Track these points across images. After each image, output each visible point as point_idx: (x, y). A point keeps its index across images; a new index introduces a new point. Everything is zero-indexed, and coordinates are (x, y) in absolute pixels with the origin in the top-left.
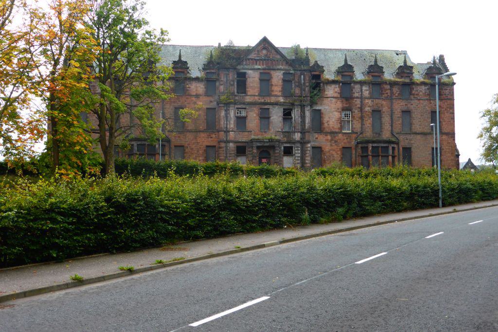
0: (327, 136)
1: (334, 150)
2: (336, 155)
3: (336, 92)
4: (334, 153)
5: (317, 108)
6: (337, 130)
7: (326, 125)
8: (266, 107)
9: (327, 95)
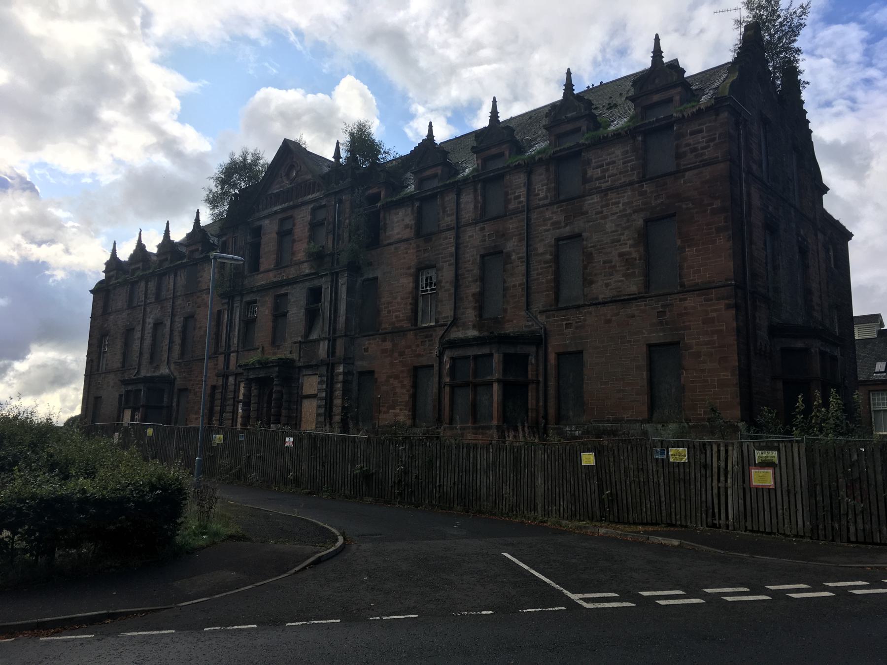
0: (384, 340)
1: (396, 377)
5: (371, 276)
6: (406, 325)
7: (384, 313)
8: (520, 350)
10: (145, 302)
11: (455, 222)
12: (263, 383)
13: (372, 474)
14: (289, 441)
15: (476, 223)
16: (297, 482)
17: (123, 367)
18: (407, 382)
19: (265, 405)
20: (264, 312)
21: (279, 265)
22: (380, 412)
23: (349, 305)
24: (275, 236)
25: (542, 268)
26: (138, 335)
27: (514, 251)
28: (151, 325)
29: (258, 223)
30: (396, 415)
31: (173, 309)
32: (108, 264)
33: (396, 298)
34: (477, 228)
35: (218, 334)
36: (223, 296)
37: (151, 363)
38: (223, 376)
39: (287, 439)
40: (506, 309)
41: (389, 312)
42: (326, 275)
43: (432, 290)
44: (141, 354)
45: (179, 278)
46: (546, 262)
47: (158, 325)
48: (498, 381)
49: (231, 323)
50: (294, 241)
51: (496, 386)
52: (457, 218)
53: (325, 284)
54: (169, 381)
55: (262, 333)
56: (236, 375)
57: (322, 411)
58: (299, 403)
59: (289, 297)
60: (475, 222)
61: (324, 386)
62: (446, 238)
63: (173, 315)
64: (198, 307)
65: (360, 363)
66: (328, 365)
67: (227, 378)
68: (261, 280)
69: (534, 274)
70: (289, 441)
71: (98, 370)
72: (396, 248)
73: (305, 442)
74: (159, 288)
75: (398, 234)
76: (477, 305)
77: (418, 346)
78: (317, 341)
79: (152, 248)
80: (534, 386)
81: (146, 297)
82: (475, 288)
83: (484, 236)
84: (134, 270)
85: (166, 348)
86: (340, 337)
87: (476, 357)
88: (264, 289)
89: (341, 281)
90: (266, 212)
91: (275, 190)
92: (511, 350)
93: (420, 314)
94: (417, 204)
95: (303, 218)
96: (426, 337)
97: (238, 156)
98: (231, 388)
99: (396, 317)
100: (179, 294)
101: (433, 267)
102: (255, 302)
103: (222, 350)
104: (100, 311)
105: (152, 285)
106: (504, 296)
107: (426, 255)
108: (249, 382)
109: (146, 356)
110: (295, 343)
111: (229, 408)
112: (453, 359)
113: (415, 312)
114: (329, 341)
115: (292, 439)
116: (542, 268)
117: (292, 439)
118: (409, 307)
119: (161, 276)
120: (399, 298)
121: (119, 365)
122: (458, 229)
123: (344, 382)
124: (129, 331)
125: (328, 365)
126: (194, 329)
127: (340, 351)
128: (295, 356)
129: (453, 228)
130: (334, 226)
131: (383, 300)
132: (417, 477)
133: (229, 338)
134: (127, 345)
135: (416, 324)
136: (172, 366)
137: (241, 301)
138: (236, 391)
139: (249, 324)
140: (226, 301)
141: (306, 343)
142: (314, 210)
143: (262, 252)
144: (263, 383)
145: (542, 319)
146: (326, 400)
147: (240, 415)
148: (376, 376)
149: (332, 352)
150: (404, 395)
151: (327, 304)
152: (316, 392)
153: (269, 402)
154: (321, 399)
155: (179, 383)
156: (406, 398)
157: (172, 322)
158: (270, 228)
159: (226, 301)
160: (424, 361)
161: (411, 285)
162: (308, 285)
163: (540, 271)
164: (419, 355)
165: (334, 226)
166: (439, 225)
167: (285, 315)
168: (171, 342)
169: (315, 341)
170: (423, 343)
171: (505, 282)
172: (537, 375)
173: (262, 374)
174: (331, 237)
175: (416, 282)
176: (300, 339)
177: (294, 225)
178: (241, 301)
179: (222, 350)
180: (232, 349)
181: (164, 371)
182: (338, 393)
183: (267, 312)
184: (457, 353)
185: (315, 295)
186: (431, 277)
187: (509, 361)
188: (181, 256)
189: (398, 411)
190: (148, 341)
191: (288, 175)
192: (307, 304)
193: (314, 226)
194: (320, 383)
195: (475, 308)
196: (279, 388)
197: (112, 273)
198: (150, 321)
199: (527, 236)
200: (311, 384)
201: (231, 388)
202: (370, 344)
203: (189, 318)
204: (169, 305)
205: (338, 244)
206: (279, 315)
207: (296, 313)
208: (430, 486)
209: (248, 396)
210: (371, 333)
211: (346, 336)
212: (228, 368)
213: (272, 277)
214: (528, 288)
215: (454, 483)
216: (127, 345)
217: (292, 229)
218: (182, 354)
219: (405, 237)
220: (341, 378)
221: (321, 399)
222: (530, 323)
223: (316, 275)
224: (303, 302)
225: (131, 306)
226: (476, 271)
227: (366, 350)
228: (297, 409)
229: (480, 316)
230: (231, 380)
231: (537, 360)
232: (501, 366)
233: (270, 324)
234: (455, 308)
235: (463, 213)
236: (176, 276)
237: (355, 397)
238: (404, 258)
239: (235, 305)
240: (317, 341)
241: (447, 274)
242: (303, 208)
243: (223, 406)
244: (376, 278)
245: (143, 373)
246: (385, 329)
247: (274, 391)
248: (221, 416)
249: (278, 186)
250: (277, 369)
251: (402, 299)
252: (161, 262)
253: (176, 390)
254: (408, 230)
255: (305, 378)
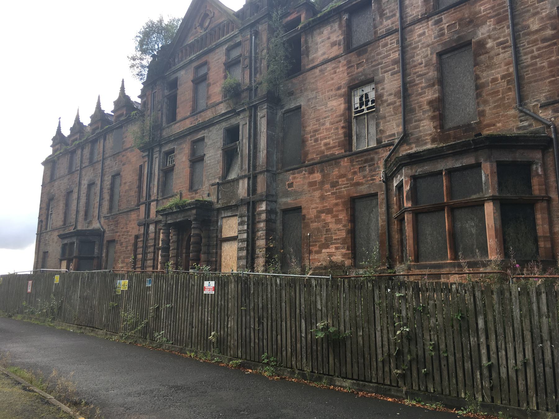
0: (312, 172)
1: (329, 211)
2: (332, 226)
3: (333, 44)
4: (329, 219)
5: (293, 106)
6: (337, 152)
7: (310, 142)
8: (520, 156)
9: (313, 60)
10: (81, 166)
11: (398, 23)
12: (181, 228)
13: (344, 339)
14: (209, 286)
15: (428, 18)
16: (221, 345)
17: (64, 224)
18: (343, 216)
19: (184, 251)
20: (182, 160)
21: (195, 112)
22: (310, 252)
23: (270, 139)
24: (191, 83)
25: (538, 49)
26: (75, 196)
27: (489, 37)
28: (86, 186)
29: (173, 77)
30: (330, 255)
31: (103, 170)
32: (54, 139)
33: (324, 124)
34: (430, 23)
35: (140, 187)
36: (142, 149)
37: (86, 219)
38: (144, 225)
39: (206, 284)
40: (483, 111)
41: (316, 140)
42: (244, 110)
43: (368, 109)
44: (77, 212)
45: (107, 141)
46: (544, 40)
47: (91, 185)
48: (493, 199)
49: (151, 173)
50: (209, 85)
51: (489, 209)
52: (402, 18)
53: (242, 121)
54: (99, 234)
55: (180, 181)
56: (157, 223)
57: (244, 253)
58: (218, 247)
59: (206, 140)
60: (426, 17)
61: (245, 227)
62: (386, 45)
63: (103, 175)
64: (123, 165)
65: (284, 200)
66: (248, 203)
67: (148, 227)
68: (177, 128)
69: (527, 59)
70: (209, 286)
71: (46, 229)
72: (320, 71)
73: (232, 286)
74: (92, 153)
75: (324, 54)
76: (437, 113)
77: (355, 173)
78: (236, 180)
79: (86, 121)
80: (545, 204)
81: (81, 162)
82: (431, 95)
83: (442, 29)
84: (73, 141)
85: (97, 205)
86: (261, 173)
87: (451, 172)
88: (181, 137)
89: (260, 114)
90: (182, 64)
91: (190, 40)
92: (507, 157)
93: (354, 138)
94: (345, 17)
95: (217, 59)
96: (366, 161)
97: (156, 20)
98: (152, 235)
99: (326, 144)
100: (107, 155)
101: (369, 81)
102: (173, 151)
103: (143, 200)
104: (48, 179)
105: (87, 152)
106: (479, 95)
107: (360, 69)
108: (168, 226)
109: (82, 213)
110: (213, 185)
111: (150, 256)
112: (414, 179)
113: (348, 135)
114: (249, 179)
115: (212, 283)
116: (538, 49)
117: (212, 283)
118: (341, 131)
119: (94, 142)
120: (328, 125)
121: (61, 223)
122: (404, 28)
123: (268, 221)
124: (69, 193)
125: (248, 203)
126: (120, 185)
127: (261, 188)
128: (213, 198)
129: (396, 31)
130: (251, 60)
131: (308, 129)
132: (436, 347)
133: (149, 189)
134: (67, 205)
135: (350, 149)
136: (102, 220)
137: (160, 151)
138: (156, 239)
139: (168, 172)
140: (146, 154)
141: (225, 184)
142: (229, 50)
143: (178, 102)
144: (181, 228)
145: (546, 115)
146: (248, 241)
147: (160, 260)
148: (304, 212)
149: (252, 189)
150: (338, 228)
151: (245, 141)
152: (236, 234)
153: (188, 248)
154: (242, 241)
155: (108, 235)
156: (343, 234)
157: (102, 181)
158: (185, 78)
159: (146, 154)
160: (364, 190)
161: (343, 107)
162: (225, 125)
163: (536, 53)
164: (358, 184)
165: (251, 60)
166: (376, 33)
167: (201, 159)
168: (101, 199)
169: (233, 181)
170: (362, 169)
171: (477, 78)
172: (547, 191)
173: (180, 218)
174: (247, 72)
175: (349, 102)
176: (217, 181)
177: (209, 69)
178: (160, 151)
179: (143, 200)
180: (152, 198)
181: (96, 225)
182: (261, 233)
183: (184, 159)
184: (419, 170)
185: (232, 134)
186: (367, 95)
187: (504, 171)
188: (109, 122)
189: (333, 250)
190: (83, 200)
191: (201, 25)
192: (224, 145)
193: (230, 66)
194: (241, 224)
195: (433, 118)
196: (197, 232)
197: (57, 147)
198: (85, 183)
199: (512, 13)
200: (231, 226)
201: (152, 235)
202: (294, 178)
203: (117, 175)
204: (99, 166)
205: (255, 77)
206: (196, 160)
207: (213, 155)
208: (468, 365)
209: (167, 242)
210: (295, 166)
211: (268, 171)
212: (149, 216)
213: (188, 124)
214: (520, 78)
215: (525, 364)
216: (67, 205)
217: (206, 74)
218: (111, 209)
219: (332, 55)
220: (263, 216)
221: (242, 241)
222: (526, 124)
223: (234, 113)
224: (220, 143)
225: (71, 172)
226: (432, 74)
227: (291, 185)
228: (216, 253)
229: (442, 126)
230: (152, 228)
231: (545, 170)
232: (496, 178)
233: (188, 170)
234: (405, 122)
235: (409, 10)
236: (105, 140)
237: (284, 232)
238: (333, 79)
239: (155, 156)
240: (236, 180)
241: (391, 84)
242: (218, 50)
243: (145, 254)
244: (299, 107)
245: (79, 228)
246: (313, 159)
247: (193, 233)
248: (135, 258)
249: (192, 37)
250: (194, 212)
251: (332, 124)
252: (94, 130)
253: (105, 242)
254: (336, 48)
255: (224, 220)
